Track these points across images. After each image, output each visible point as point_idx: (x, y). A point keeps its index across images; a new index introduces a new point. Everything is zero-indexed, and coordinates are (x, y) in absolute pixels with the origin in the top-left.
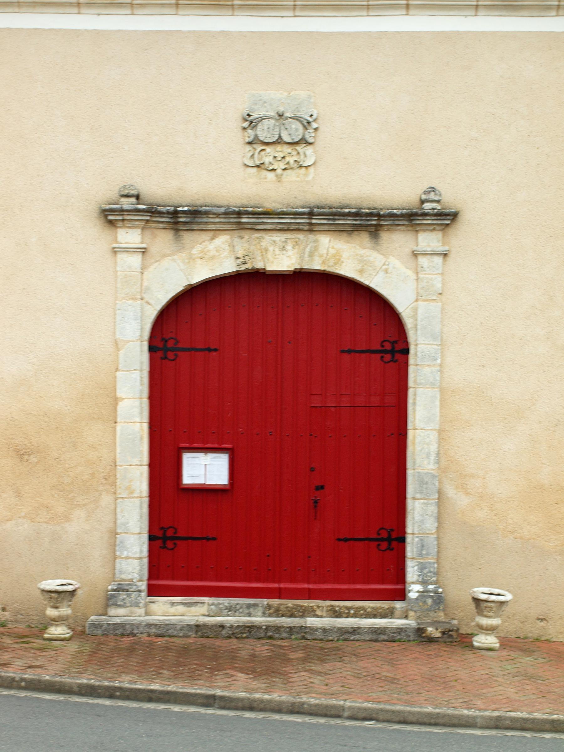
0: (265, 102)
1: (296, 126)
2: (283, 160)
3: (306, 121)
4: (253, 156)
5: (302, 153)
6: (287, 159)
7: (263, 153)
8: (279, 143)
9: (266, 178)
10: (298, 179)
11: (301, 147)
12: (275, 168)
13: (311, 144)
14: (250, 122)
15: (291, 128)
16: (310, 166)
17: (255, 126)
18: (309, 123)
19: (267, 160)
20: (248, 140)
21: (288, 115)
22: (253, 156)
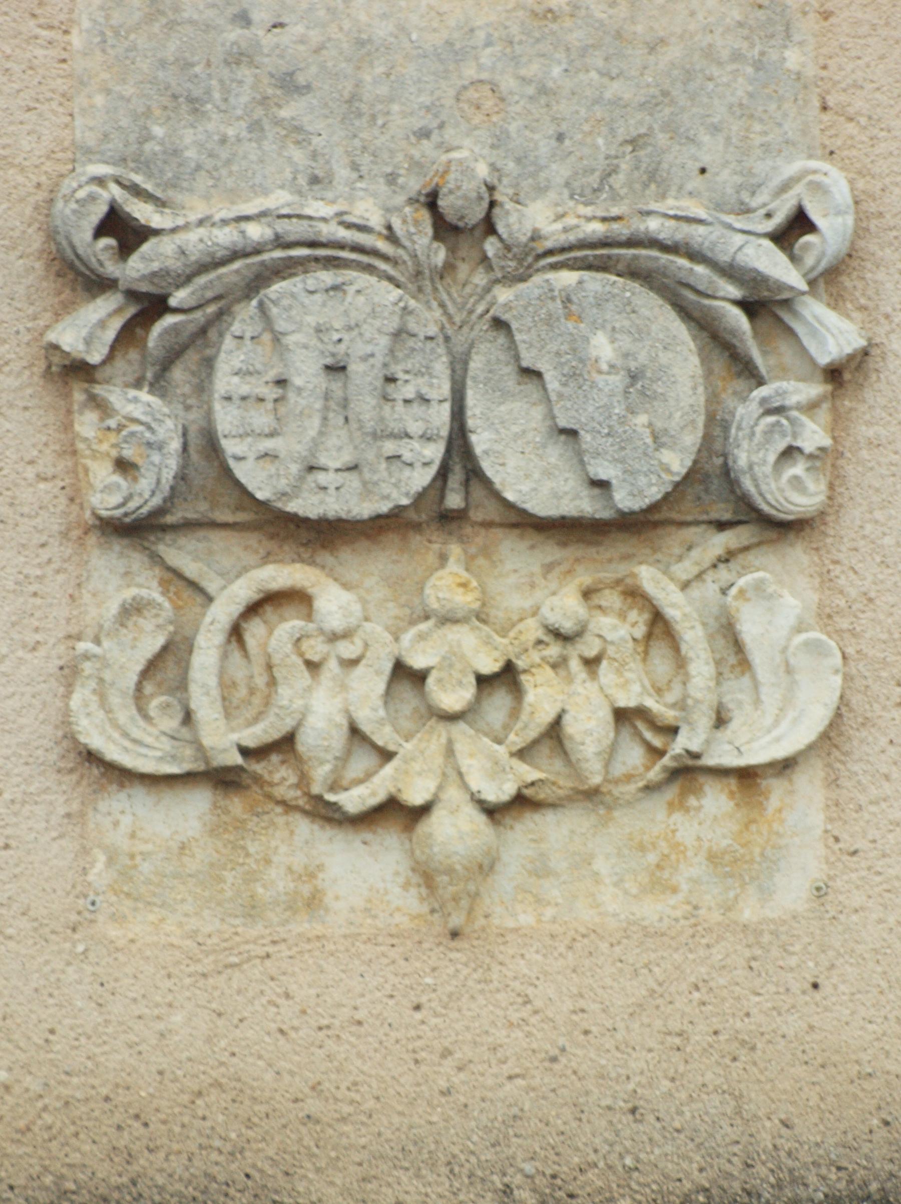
0: (289, 84)
1: (630, 339)
2: (498, 704)
3: (734, 291)
4: (167, 665)
5: (694, 637)
6: (542, 697)
7: (279, 634)
8: (449, 520)
9: (314, 903)
10: (653, 910)
11: (685, 569)
12: (415, 797)
13: (782, 528)
14: (140, 298)
15: (578, 373)
16: (785, 766)
17: (201, 340)
18: (764, 304)
19: (320, 711)
20: (108, 494)
21: (537, 217)
22: (167, 665)
